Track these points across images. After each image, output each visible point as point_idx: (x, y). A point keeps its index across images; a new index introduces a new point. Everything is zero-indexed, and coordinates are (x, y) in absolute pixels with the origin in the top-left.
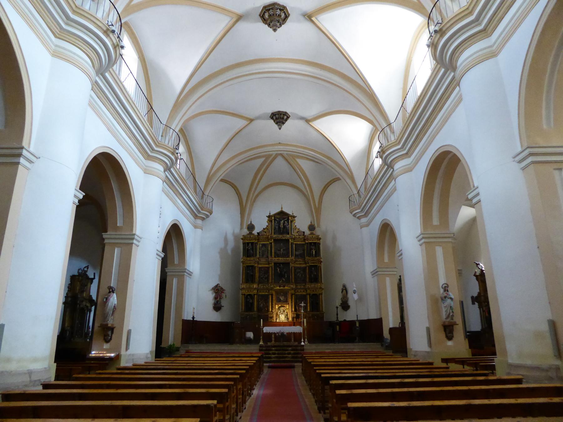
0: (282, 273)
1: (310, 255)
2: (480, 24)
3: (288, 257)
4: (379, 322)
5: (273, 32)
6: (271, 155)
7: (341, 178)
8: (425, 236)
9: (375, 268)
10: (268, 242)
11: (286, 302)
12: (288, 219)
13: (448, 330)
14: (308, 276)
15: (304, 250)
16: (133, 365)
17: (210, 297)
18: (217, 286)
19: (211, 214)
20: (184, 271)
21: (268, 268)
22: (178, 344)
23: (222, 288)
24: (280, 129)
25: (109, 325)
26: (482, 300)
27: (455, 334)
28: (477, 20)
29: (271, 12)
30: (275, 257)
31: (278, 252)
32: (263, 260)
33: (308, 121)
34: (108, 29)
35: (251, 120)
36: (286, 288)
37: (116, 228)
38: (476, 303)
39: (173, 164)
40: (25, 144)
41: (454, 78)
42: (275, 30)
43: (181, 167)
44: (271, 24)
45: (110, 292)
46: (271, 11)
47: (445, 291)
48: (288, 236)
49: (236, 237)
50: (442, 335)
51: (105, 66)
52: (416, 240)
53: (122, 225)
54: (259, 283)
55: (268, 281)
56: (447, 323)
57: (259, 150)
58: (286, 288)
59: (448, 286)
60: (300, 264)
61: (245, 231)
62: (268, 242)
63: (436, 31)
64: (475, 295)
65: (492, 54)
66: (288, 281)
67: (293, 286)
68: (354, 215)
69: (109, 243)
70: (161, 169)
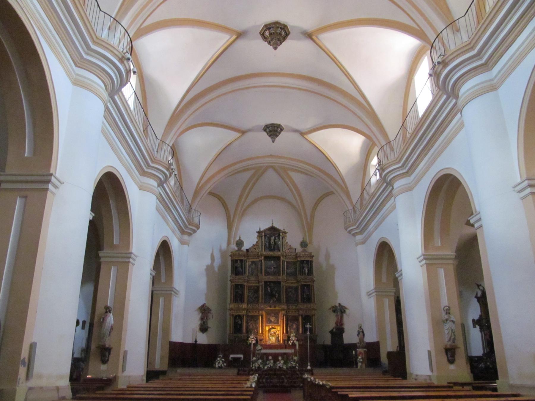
0: (272, 293)
1: (302, 273)
2: (481, 59)
3: (279, 275)
5: (273, 50)
7: (335, 192)
8: (426, 257)
10: (258, 260)
11: (277, 323)
12: (279, 235)
13: (450, 353)
15: (296, 269)
16: (128, 387)
17: (195, 321)
18: (203, 305)
19: (198, 229)
21: (258, 287)
22: (165, 367)
23: (208, 308)
24: (273, 142)
25: (107, 346)
26: (484, 323)
27: (457, 357)
28: (479, 55)
29: (272, 31)
30: (265, 275)
32: (253, 279)
33: (302, 134)
34: (123, 57)
35: (243, 132)
36: (277, 308)
37: (113, 247)
38: (477, 326)
39: (167, 178)
41: (455, 104)
42: (275, 48)
43: (129, 92)
44: (272, 43)
45: (106, 312)
46: (272, 29)
47: (447, 313)
48: (279, 253)
49: (223, 254)
51: (114, 90)
53: (118, 243)
55: (258, 300)
56: (448, 347)
58: (277, 308)
59: (449, 309)
60: (292, 282)
61: (234, 247)
62: (258, 260)
63: (439, 63)
64: (477, 317)
65: (492, 88)
66: (279, 301)
68: (349, 232)
69: (105, 262)
70: (155, 184)
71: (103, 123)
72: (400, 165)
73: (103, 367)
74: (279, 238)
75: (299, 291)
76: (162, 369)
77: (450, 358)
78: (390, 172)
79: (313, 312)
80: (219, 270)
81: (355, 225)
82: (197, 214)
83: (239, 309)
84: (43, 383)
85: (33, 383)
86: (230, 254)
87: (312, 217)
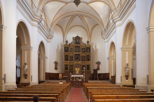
0: (77, 57)
1: (87, 52)
4: (108, 74)
6: (74, 15)
9: (109, 57)
13: (127, 77)
14: (86, 59)
15: (85, 50)
17: (53, 65)
18: (56, 62)
20: (45, 57)
21: (73, 56)
23: (57, 62)
24: (77, 7)
25: (26, 74)
30: (75, 52)
31: (76, 50)
35: (67, 3)
37: (25, 45)
39: (41, 22)
40: (3, 24)
48: (80, 45)
49: (61, 45)
50: (125, 78)
52: (120, 49)
54: (70, 61)
56: (126, 75)
57: (69, 13)
61: (65, 43)
66: (79, 60)
67: (81, 62)
70: (37, 24)
71: (17, 5)
72: (118, 17)
73: (26, 80)
74: (80, 40)
75: (86, 57)
76: (44, 80)
77: (127, 78)
78: (115, 19)
79: (90, 64)
80: (60, 50)
81: (105, 36)
82: (52, 32)
83: (67, 63)
84: (9, 84)
85: (6, 84)
86: (64, 45)
87: (91, 33)
